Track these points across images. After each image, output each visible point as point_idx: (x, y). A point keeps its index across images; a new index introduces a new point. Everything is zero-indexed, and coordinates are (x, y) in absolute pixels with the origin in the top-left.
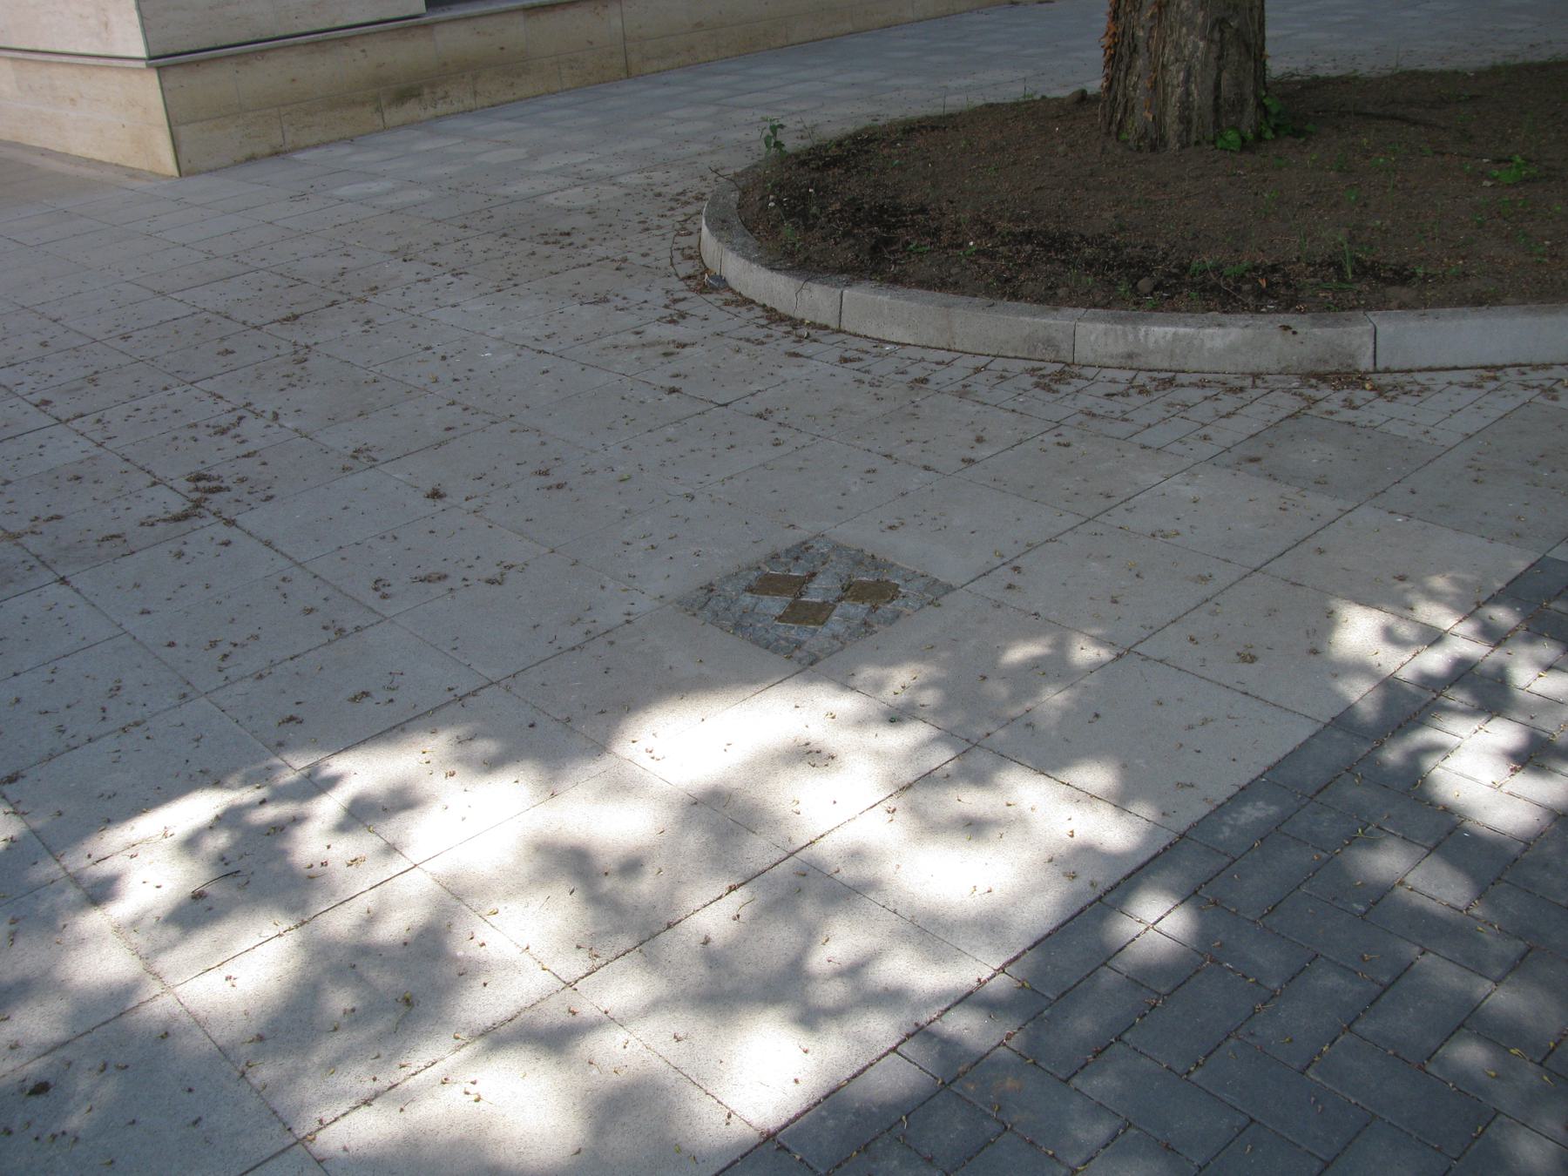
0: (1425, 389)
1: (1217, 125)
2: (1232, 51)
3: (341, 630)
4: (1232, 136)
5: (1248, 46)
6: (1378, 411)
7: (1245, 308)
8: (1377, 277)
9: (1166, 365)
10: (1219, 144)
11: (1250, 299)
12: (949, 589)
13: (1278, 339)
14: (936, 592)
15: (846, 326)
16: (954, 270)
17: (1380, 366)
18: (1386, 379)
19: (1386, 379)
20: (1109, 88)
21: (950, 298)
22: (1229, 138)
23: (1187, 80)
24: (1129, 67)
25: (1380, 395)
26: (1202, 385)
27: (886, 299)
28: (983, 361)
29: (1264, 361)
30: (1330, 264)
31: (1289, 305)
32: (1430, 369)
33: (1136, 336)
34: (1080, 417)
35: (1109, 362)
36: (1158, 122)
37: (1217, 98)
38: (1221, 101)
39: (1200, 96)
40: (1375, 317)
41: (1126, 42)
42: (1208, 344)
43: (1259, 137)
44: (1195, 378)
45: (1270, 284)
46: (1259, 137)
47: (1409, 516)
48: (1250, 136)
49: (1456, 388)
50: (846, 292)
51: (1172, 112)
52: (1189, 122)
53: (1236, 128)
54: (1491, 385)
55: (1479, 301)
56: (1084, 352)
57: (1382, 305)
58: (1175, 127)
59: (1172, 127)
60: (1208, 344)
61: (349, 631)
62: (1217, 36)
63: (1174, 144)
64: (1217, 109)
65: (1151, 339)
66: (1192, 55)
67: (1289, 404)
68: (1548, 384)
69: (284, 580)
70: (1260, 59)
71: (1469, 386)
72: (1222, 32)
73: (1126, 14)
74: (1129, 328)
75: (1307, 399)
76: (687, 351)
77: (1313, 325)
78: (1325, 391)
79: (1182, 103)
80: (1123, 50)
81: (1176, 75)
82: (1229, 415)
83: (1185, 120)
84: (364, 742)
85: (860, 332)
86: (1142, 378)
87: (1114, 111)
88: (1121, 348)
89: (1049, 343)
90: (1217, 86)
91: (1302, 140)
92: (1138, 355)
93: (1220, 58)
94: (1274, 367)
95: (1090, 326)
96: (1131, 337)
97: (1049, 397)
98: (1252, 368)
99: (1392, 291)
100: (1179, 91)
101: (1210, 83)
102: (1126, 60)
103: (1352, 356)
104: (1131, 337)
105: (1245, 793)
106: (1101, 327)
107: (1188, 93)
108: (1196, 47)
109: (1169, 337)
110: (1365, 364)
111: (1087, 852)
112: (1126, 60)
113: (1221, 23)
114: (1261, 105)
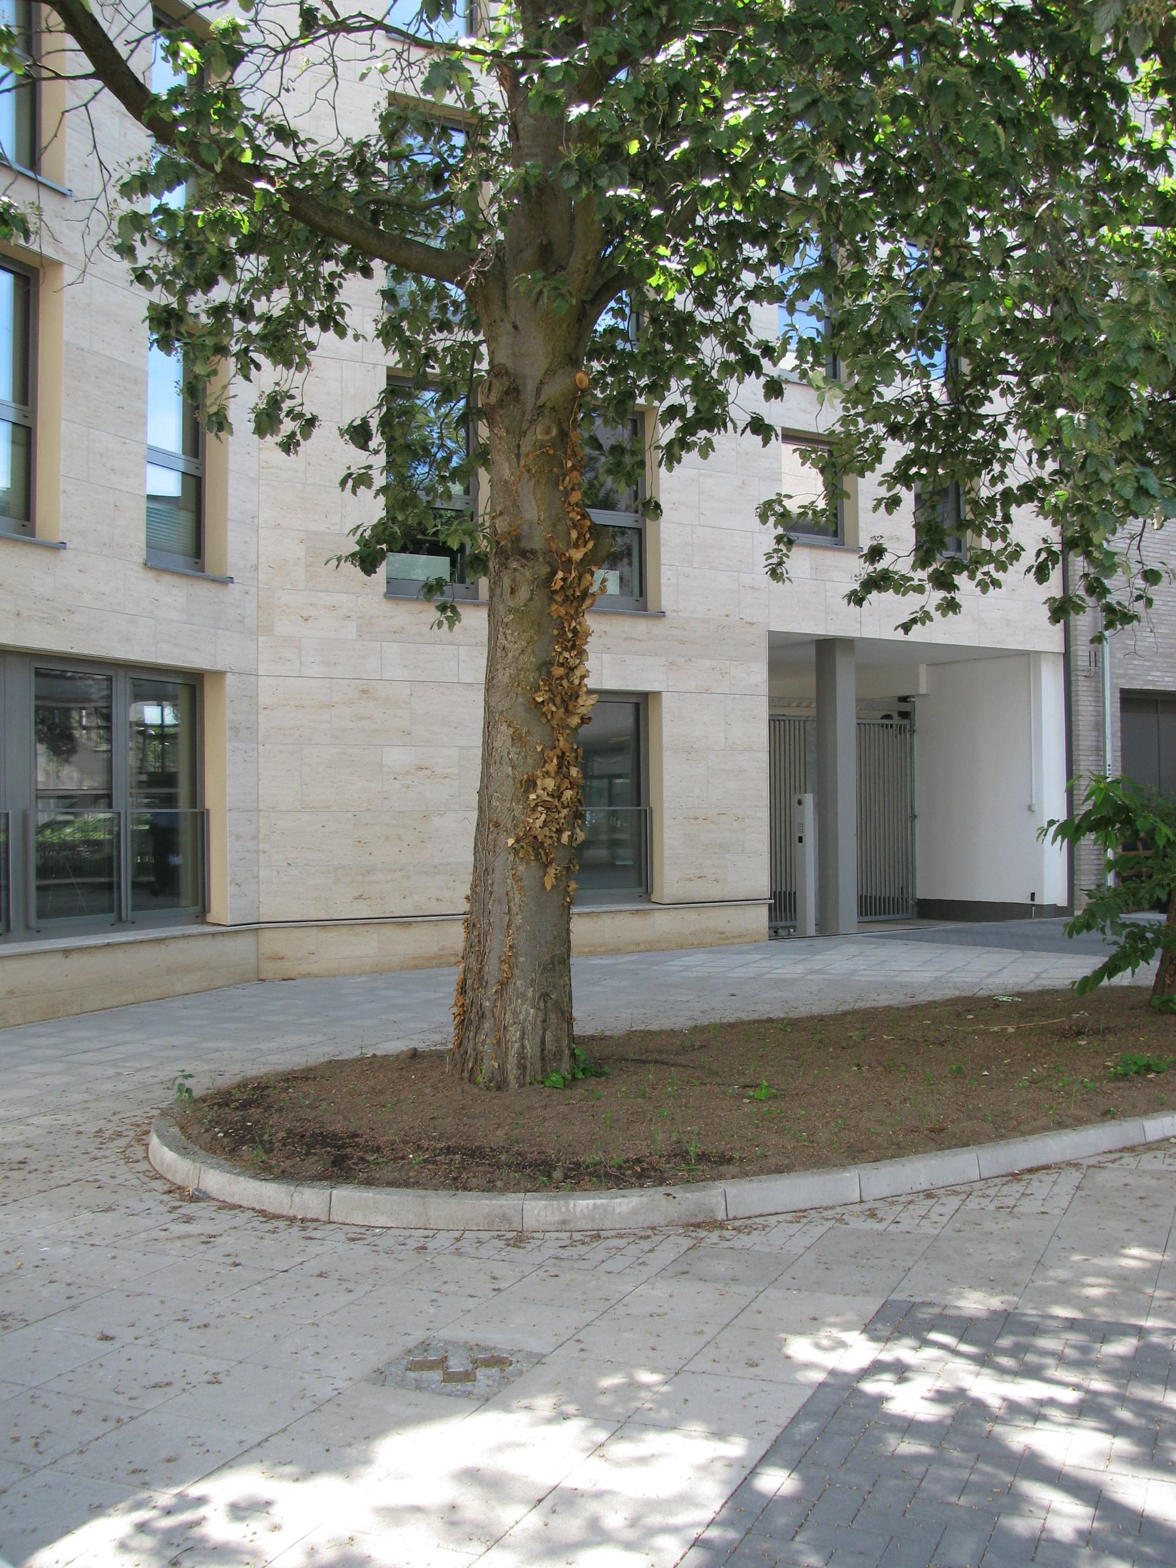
0: (764, 1227)
1: (544, 1070)
2: (553, 1016)
3: (119, 1420)
4: (555, 1077)
5: (563, 1013)
6: (743, 1240)
7: (631, 1186)
8: (710, 1161)
9: (590, 1227)
10: (547, 1084)
11: (633, 1180)
12: (544, 1356)
13: (664, 1202)
14: (539, 1359)
15: (334, 1218)
16: (412, 1174)
17: (731, 1216)
18: (737, 1223)
19: (737, 1223)
20: (460, 1045)
21: (422, 1192)
22: (554, 1079)
23: (522, 1037)
24: (478, 1029)
25: (740, 1232)
26: (621, 1236)
27: (371, 1195)
28: (458, 1234)
29: (656, 1219)
30: (676, 1155)
31: (661, 1181)
32: (762, 1216)
33: (567, 1209)
34: (552, 1261)
35: (547, 1227)
36: (502, 1069)
37: (543, 1050)
38: (546, 1052)
39: (532, 1049)
40: (721, 1185)
41: (474, 1010)
42: (618, 1210)
43: (574, 1078)
44: (613, 1233)
45: (643, 1169)
46: (574, 1078)
47: (799, 1290)
48: (569, 1077)
49: (784, 1224)
50: (335, 1192)
51: (512, 1061)
52: (525, 1067)
53: (557, 1071)
54: (804, 1220)
55: (779, 1170)
56: (530, 1223)
57: (721, 1177)
58: (515, 1072)
59: (512, 1072)
60: (618, 1210)
61: (126, 1420)
62: (542, 1005)
63: (513, 1084)
64: (543, 1058)
65: (578, 1210)
66: (525, 1020)
67: (686, 1243)
68: (838, 1216)
69: (424, 1248)
70: (570, 1020)
71: (791, 1222)
72: (545, 1002)
73: (473, 990)
74: (562, 1202)
75: (696, 1238)
76: (218, 1240)
77: (685, 1192)
78: (702, 1233)
79: (519, 1054)
80: (472, 1016)
81: (514, 1034)
82: (651, 1251)
83: (522, 1067)
84: (210, 1474)
85: (347, 1221)
86: (577, 1236)
87: (464, 1061)
88: (557, 1217)
89: (504, 1217)
90: (543, 1041)
91: (603, 1078)
92: (570, 1221)
93: (544, 1021)
94: (663, 1222)
95: (533, 1203)
96: (563, 1209)
97: (521, 1251)
98: (648, 1223)
99: (723, 1168)
100: (517, 1045)
101: (538, 1040)
102: (475, 1023)
103: (712, 1211)
104: (563, 1209)
105: (795, 1420)
106: (542, 1203)
107: (523, 1047)
108: (528, 1013)
109: (590, 1207)
110: (721, 1215)
111: (730, 1463)
112: (475, 1023)
113: (545, 996)
114: (573, 1055)
